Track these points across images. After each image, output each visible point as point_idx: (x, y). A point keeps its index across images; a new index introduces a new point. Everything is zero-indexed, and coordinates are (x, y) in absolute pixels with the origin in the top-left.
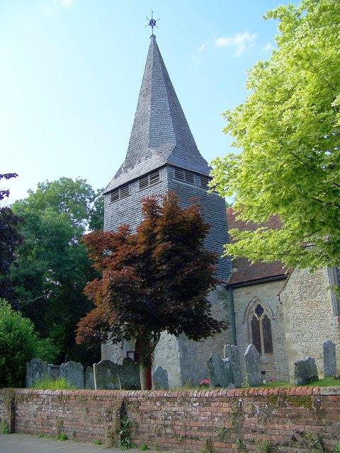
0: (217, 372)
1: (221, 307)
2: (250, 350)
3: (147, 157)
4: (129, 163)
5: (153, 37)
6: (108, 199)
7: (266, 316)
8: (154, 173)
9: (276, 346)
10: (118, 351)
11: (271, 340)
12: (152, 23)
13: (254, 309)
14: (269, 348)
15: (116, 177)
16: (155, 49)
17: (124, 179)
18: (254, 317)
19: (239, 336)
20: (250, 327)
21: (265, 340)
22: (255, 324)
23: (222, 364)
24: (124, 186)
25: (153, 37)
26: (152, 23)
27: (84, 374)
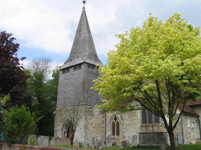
0: (95, 142)
1: (101, 117)
2: (108, 135)
3: (77, 58)
4: (70, 59)
5: (84, 8)
6: (61, 72)
7: (117, 121)
8: (80, 65)
9: (121, 133)
10: (61, 131)
11: (119, 131)
12: (84, 2)
13: (113, 118)
14: (118, 134)
15: (65, 63)
16: (84, 15)
17: (68, 65)
18: (113, 121)
19: (107, 128)
20: (112, 125)
21: (117, 130)
22: (114, 124)
23: (97, 140)
24: (68, 68)
25: (84, 8)
26: (84, 2)
27: (81, 28)
